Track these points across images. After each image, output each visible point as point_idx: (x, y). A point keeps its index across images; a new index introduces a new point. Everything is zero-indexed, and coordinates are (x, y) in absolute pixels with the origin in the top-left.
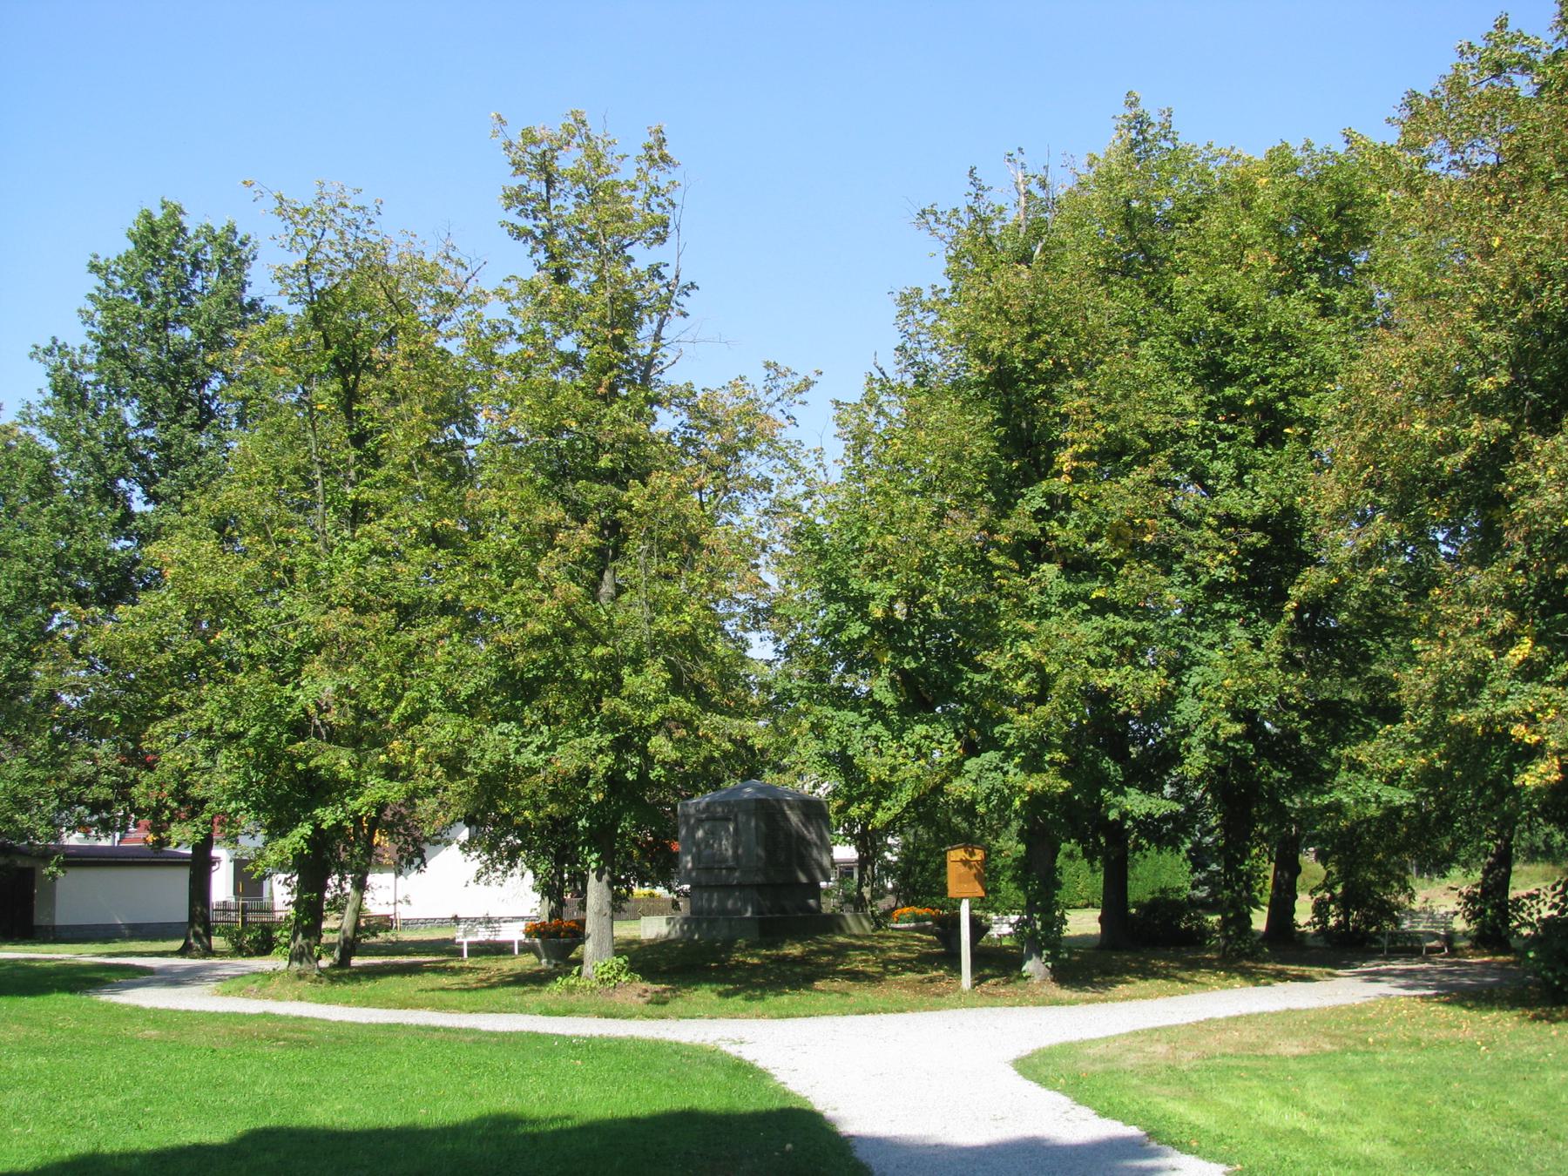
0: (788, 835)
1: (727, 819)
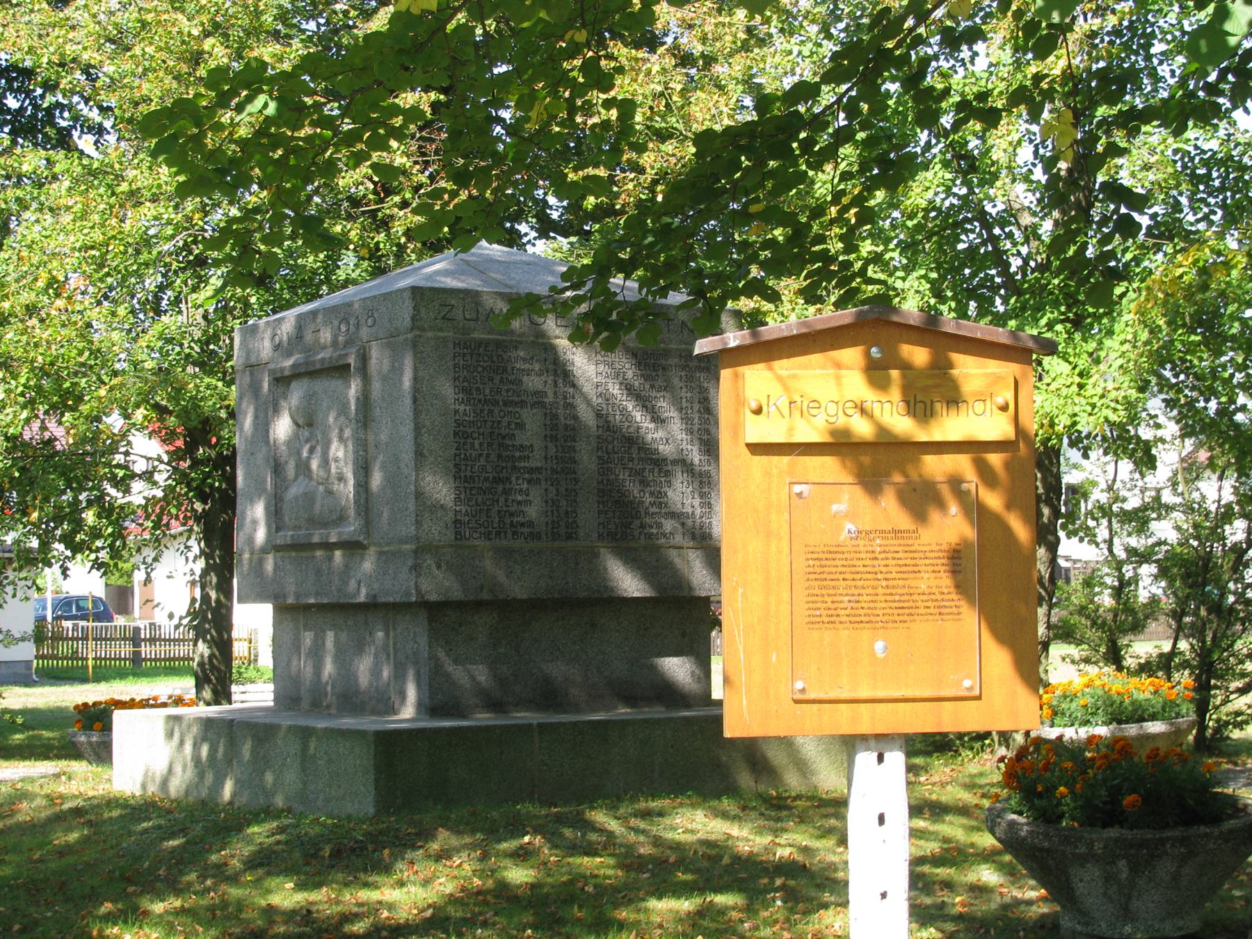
0: (562, 430)
1: (340, 370)
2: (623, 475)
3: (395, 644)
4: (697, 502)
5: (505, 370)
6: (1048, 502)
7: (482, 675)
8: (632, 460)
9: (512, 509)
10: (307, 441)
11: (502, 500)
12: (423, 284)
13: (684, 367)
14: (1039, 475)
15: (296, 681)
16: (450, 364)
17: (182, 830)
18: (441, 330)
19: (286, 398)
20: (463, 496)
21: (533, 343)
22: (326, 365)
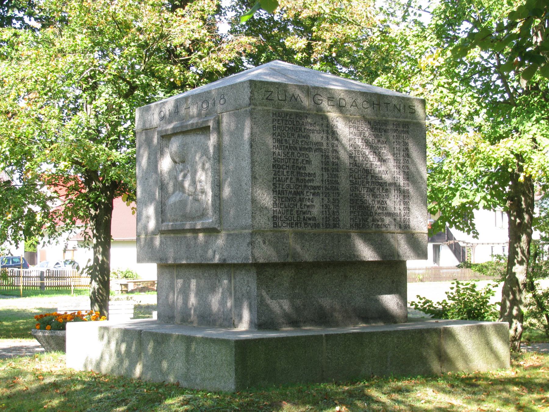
0: (331, 166)
1: (204, 130)
2: (364, 192)
3: (235, 287)
4: (402, 207)
5: (300, 130)
6: (528, 212)
7: (286, 305)
8: (368, 182)
9: (304, 210)
10: (181, 171)
11: (299, 204)
12: (255, 79)
13: (396, 131)
14: (523, 199)
15: (172, 307)
16: (271, 125)
17: (123, 401)
18: (266, 106)
19: (168, 147)
20: (277, 202)
21: (316, 114)
22: (194, 127)
